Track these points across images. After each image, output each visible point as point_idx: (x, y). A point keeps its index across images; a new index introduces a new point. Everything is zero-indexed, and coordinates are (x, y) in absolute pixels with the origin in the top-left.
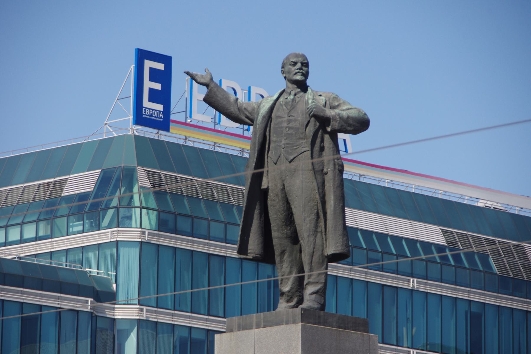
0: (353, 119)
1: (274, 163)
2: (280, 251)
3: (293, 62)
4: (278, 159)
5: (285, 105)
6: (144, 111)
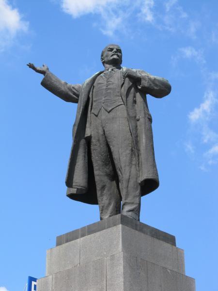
0: (158, 81)
1: (95, 115)
2: (100, 186)
3: (111, 48)
4: (99, 112)
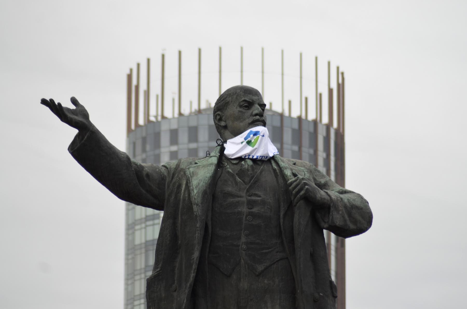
5: (237, 174)
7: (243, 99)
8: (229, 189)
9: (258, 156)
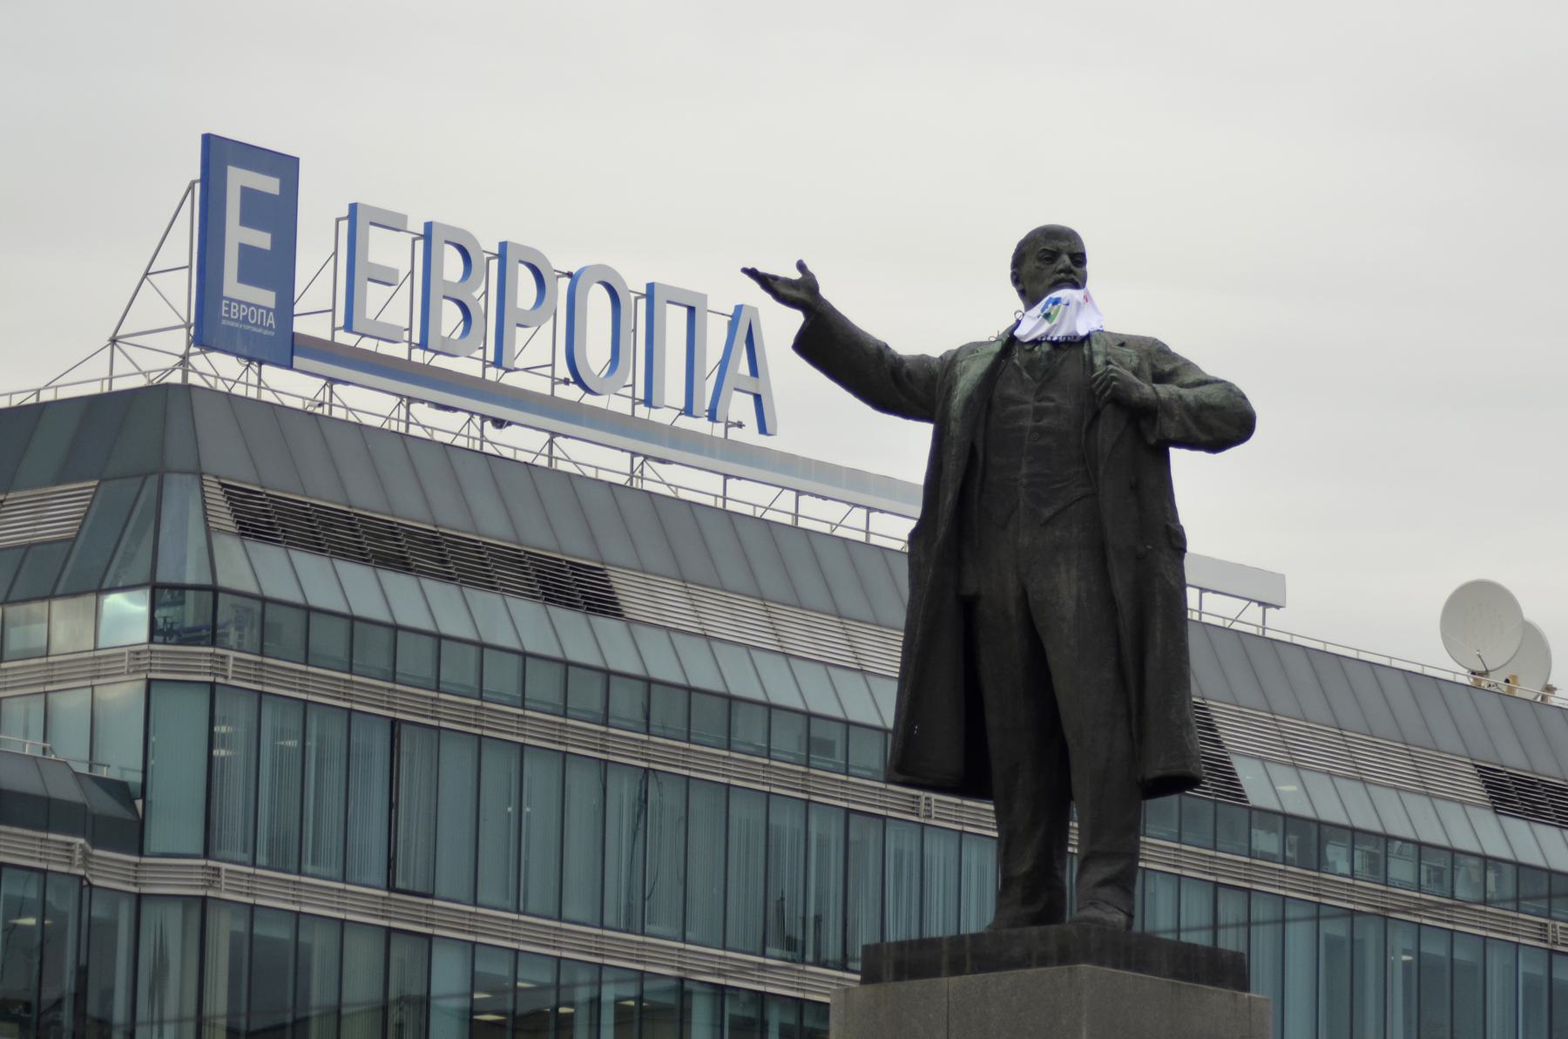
5: (1026, 367)
6: (224, 308)
7: (1042, 248)
8: (1012, 391)
9: (1058, 337)
